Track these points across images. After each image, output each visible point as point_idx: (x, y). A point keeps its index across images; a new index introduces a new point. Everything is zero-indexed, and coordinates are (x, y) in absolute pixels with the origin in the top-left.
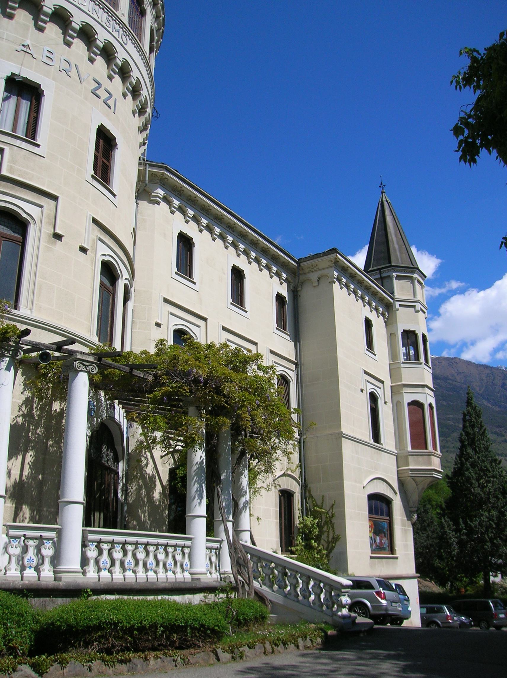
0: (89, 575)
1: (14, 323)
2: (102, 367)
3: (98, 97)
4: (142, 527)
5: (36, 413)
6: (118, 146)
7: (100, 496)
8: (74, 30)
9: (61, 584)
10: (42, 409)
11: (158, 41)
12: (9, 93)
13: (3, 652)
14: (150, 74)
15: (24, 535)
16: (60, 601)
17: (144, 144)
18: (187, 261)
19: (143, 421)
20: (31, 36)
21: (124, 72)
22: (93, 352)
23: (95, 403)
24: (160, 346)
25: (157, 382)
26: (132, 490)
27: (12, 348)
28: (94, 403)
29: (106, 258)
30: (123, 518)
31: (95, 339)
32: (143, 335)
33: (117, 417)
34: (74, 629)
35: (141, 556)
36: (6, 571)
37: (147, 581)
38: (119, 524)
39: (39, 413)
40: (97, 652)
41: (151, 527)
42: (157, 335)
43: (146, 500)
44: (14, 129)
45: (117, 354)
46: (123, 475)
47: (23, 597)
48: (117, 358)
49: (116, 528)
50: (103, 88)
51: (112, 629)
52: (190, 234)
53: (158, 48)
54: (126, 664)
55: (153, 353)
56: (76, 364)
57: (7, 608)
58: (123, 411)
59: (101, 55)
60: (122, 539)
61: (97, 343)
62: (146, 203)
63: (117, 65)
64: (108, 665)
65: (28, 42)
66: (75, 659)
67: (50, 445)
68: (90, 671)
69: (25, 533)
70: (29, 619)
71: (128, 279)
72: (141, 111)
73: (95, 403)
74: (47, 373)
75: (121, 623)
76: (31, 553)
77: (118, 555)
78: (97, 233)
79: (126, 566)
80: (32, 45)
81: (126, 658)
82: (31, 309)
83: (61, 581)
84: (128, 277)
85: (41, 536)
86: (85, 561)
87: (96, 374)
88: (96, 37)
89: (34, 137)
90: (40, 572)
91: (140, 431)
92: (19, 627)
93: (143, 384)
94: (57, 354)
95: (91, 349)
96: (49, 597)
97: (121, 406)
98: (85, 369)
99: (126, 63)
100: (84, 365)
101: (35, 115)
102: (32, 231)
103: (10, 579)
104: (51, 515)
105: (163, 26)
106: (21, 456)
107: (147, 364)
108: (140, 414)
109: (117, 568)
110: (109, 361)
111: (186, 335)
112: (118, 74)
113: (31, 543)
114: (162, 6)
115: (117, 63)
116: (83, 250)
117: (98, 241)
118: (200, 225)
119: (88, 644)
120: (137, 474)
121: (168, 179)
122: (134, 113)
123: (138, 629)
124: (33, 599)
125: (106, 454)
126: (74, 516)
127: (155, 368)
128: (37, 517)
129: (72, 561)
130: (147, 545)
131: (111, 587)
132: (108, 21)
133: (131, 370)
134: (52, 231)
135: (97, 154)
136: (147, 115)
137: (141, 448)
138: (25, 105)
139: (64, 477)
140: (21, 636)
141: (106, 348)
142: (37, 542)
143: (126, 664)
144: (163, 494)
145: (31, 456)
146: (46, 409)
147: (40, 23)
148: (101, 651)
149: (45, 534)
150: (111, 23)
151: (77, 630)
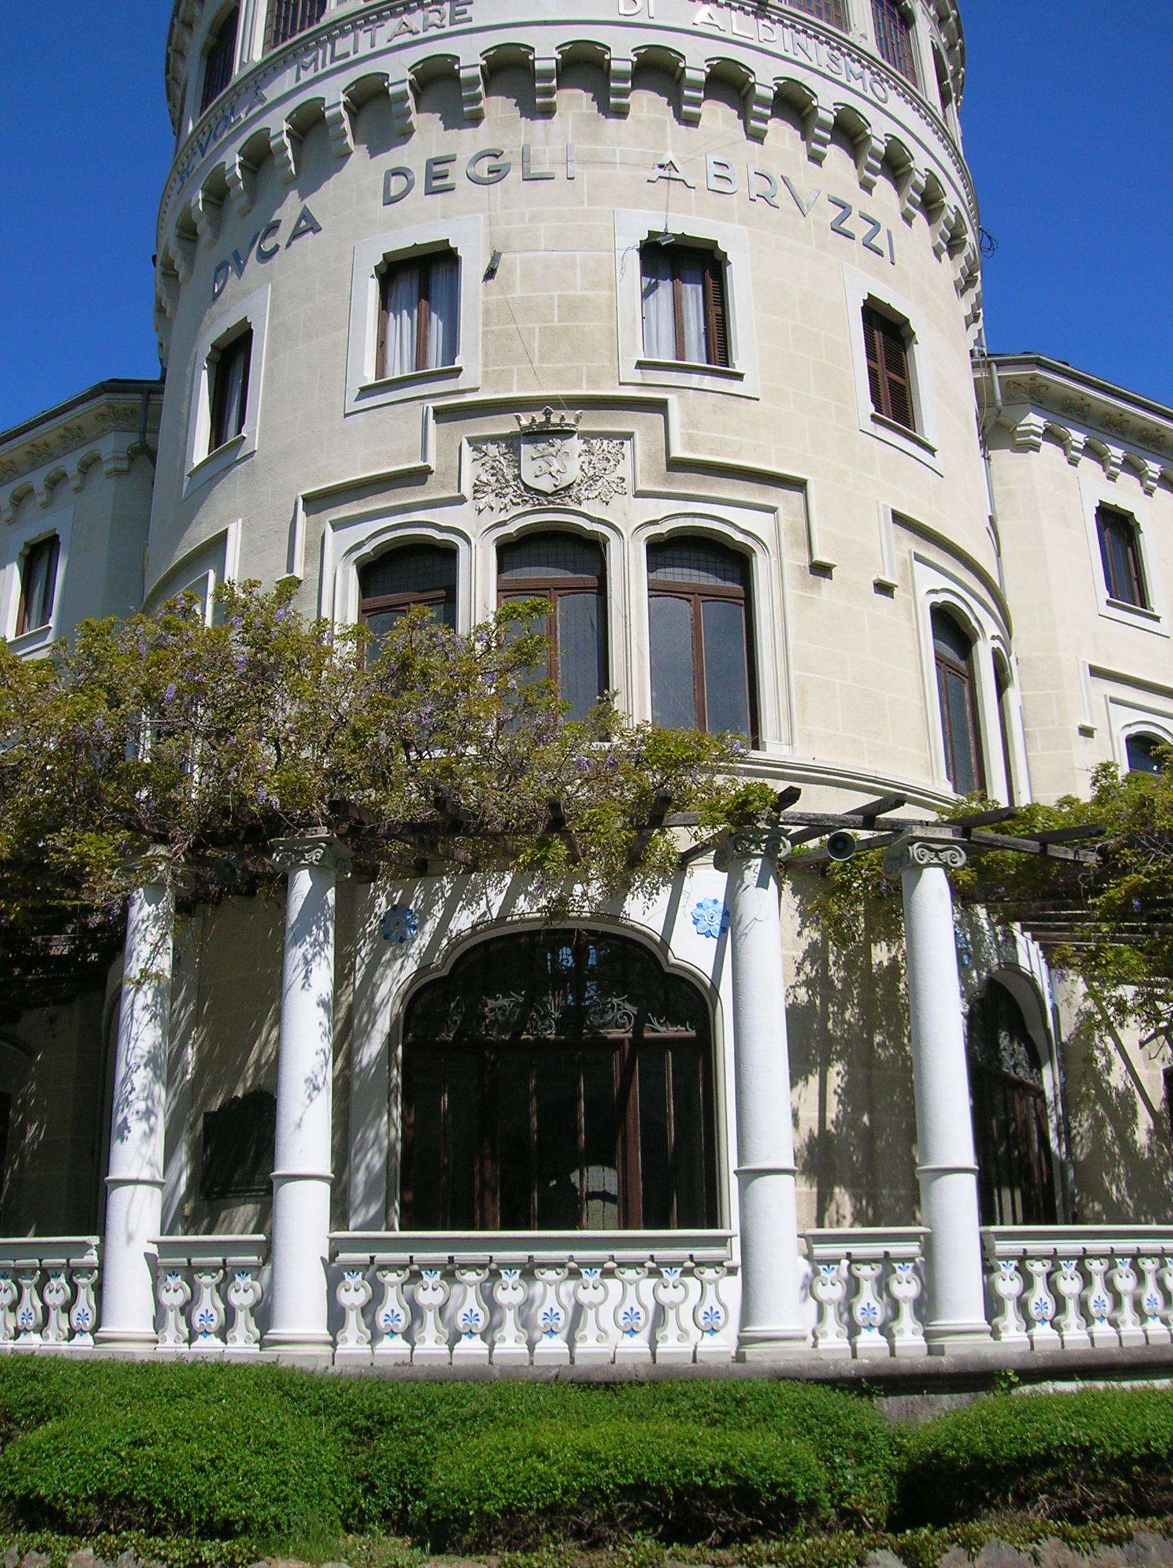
0: (1005, 1337)
1: (760, 780)
2: (974, 849)
3: (849, 236)
4: (1115, 1213)
5: (836, 974)
6: (918, 337)
7: (1009, 1150)
8: (762, 102)
9: (945, 1362)
10: (849, 965)
12: (652, 277)
13: (831, 1523)
15: (849, 1255)
16: (946, 1401)
17: (976, 318)
18: (1130, 573)
19: (1091, 965)
20: (675, 142)
21: (895, 165)
22: (946, 818)
23: (968, 936)
24: (1104, 781)
25: (1111, 866)
26: (1081, 1130)
27: (765, 837)
28: (964, 936)
29: (940, 598)
30: (1068, 1198)
31: (945, 788)
32: (1056, 761)
33: (1023, 961)
34: (988, 1466)
35: (1126, 1283)
36: (816, 1338)
37: (1121, 1344)
38: (1060, 1213)
39: (842, 974)
40: (1049, 1517)
41: (1138, 1212)
42: (1091, 755)
43: (1117, 1151)
44: (680, 351)
45: (1005, 815)
46: (1055, 1096)
47: (860, 1395)
48: (1005, 823)
49: (1055, 1223)
50: (855, 213)
51: (1077, 1463)
52: (1125, 504)
53: (960, 89)
54: (1122, 1546)
55: (1089, 800)
56: (914, 850)
57: (830, 1422)
58: (1035, 947)
60: (1074, 1246)
61: (954, 796)
62: (1006, 453)
64: (1078, 1549)
65: (668, 157)
66: (997, 1534)
67: (878, 1044)
68: (1037, 1562)
69: (652, 1253)
70: (881, 1444)
71: (998, 638)
72: (954, 244)
73: (968, 936)
74: (849, 880)
75: (1098, 1447)
77: (1070, 1285)
78: (910, 543)
79: (1093, 1310)
81: (1120, 1532)
82: (791, 743)
83: (943, 1354)
84: (997, 633)
85: (887, 1254)
86: (993, 1306)
87: (962, 868)
88: (814, 103)
89: (725, 359)
90: (894, 1336)
91: (1081, 988)
92: (860, 1464)
93: (1076, 877)
94: (864, 835)
95: (942, 811)
96: (919, 1392)
97: (1028, 934)
98: (936, 861)
99: (894, 144)
100: (931, 850)
102: (762, 569)
103: (827, 1357)
104: (901, 1205)
106: (817, 1077)
107: (1079, 829)
108: (1079, 948)
109: (1072, 1316)
110: (987, 833)
111: (1157, 744)
112: (882, 172)
113: (865, 1271)
115: (873, 149)
116: (884, 588)
117: (915, 563)
118: (1145, 478)
119: (1024, 1499)
120: (1088, 1090)
121: (1047, 387)
122: (937, 253)
123: (1142, 1461)
124: (884, 1400)
125: (1011, 1052)
126: (956, 1200)
127: (1101, 833)
128: (870, 1212)
129: (963, 1305)
130: (1136, 1256)
131: (1063, 1363)
132: (834, 60)
133: (1044, 846)
134: (807, 559)
135: (873, 365)
136: (967, 250)
137: (1091, 1028)
138: (692, 294)
139: (923, 1114)
140: (868, 1486)
141: (974, 805)
142: (878, 1268)
143: (1122, 1546)
144: (1156, 1132)
145: (838, 1074)
146: (857, 963)
147: (685, 108)
148: (1056, 1515)
149: (896, 1249)
150: (841, 62)
151: (997, 1467)
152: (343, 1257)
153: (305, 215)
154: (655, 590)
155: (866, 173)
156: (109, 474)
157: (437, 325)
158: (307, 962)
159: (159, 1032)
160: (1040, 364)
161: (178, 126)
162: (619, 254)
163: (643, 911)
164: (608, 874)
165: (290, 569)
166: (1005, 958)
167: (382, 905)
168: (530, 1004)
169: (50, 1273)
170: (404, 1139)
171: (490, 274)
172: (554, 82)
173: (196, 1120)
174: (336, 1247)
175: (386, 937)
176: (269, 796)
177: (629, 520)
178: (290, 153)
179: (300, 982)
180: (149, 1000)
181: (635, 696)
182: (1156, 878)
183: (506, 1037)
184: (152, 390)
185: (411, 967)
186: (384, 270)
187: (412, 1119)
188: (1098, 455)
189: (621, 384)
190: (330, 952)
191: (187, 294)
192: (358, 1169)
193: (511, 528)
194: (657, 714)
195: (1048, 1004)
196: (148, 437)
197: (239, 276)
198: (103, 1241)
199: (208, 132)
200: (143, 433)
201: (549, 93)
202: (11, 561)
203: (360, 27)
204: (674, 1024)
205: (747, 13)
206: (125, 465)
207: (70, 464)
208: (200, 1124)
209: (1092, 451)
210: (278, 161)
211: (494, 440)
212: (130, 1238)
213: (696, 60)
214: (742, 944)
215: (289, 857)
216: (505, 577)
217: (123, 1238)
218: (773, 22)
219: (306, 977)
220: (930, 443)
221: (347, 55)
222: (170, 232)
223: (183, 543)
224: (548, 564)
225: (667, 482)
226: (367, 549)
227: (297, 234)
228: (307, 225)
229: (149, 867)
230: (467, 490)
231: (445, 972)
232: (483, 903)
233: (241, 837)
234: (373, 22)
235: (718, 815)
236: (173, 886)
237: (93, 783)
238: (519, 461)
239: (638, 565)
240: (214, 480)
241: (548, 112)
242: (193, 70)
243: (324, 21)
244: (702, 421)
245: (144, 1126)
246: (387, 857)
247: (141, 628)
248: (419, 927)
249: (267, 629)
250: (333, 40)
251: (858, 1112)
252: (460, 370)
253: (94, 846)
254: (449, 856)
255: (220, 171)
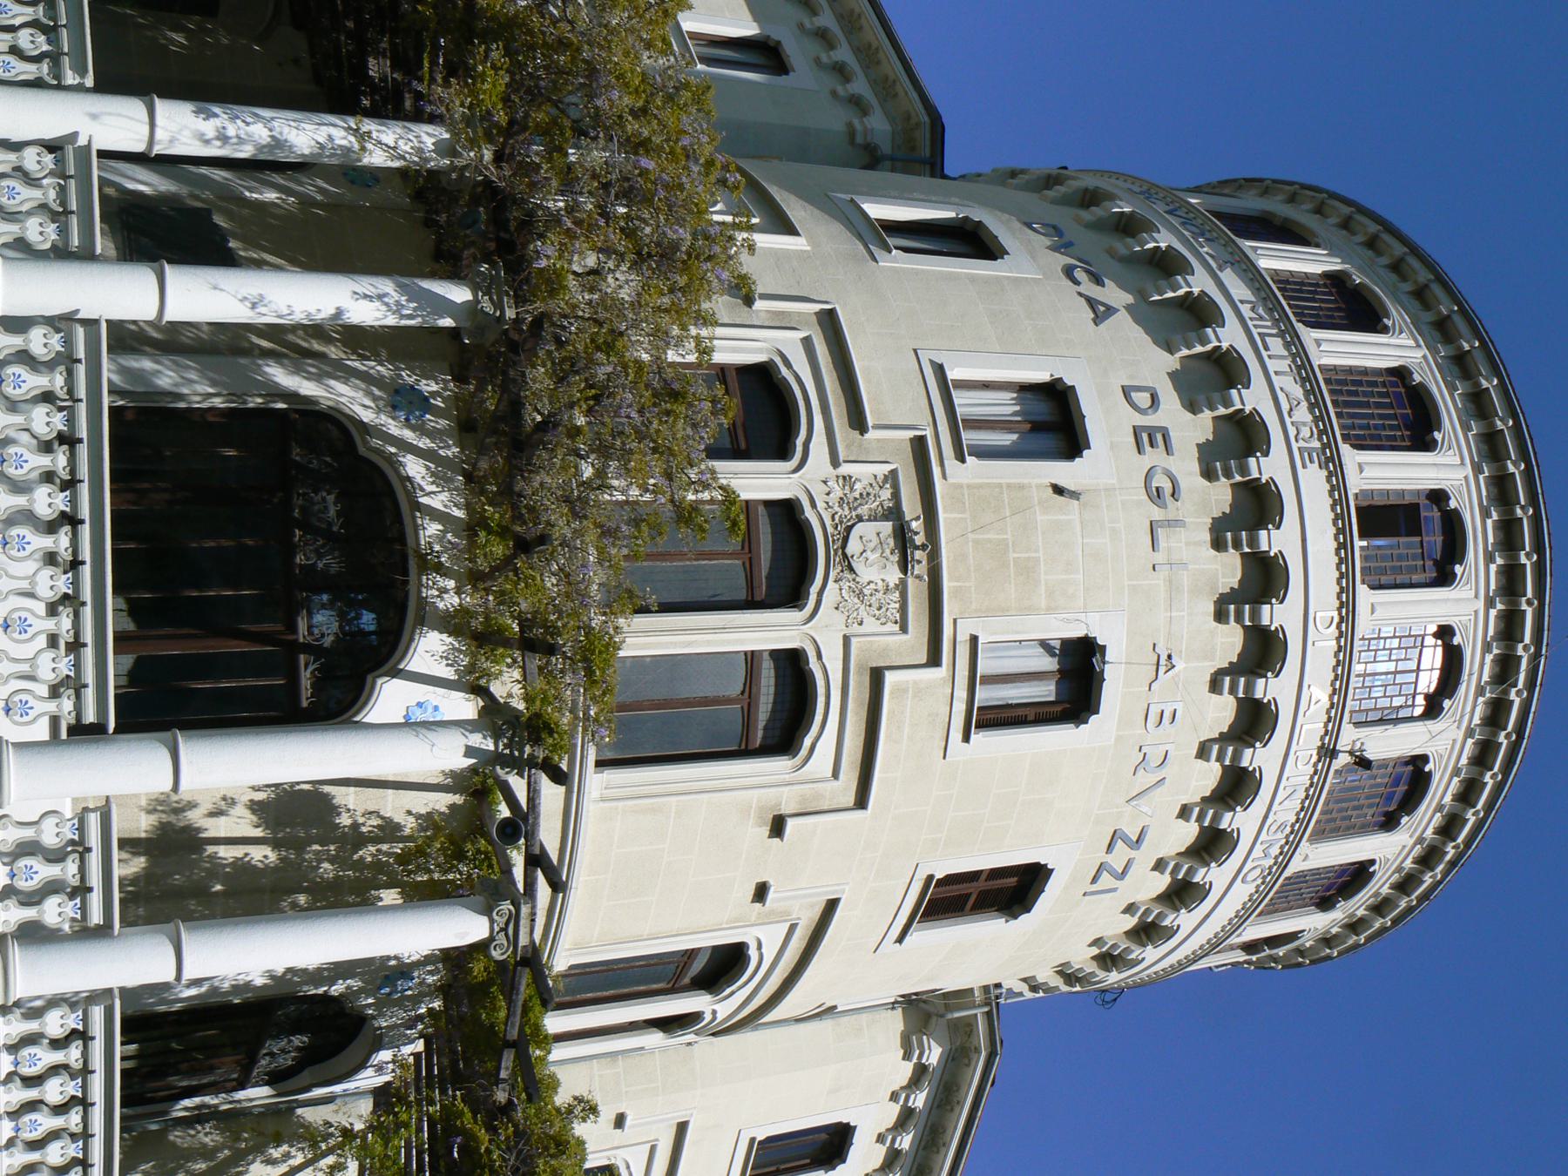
2: (504, 974)
5: (367, 853)
8: (1237, 756)
10: (378, 866)
11: (1275, 959)
14: (1196, 958)
17: (1034, 989)
20: (1195, 669)
21: (1182, 893)
25: (496, 1115)
29: (753, 953)
44: (990, 680)
46: (239, 1101)
50: (1133, 854)
56: (506, 906)
59: (1202, 829)
62: (900, 1026)
63: (1191, 871)
65: (1180, 665)
72: (1108, 960)
76: (45, 871)
78: (807, 918)
79: (26, 1118)
80: (1177, 675)
82: (603, 800)
84: (720, 1017)
88: (1238, 809)
89: (982, 725)
99: (1201, 892)
101: (1031, 718)
105: (1313, 962)
112: (1174, 881)
114: (1356, 946)
116: (761, 892)
120: (246, 1140)
121: (968, 1065)
122: (1097, 942)
125: (283, 1049)
126: (141, 963)
127: (530, 1099)
132: (1281, 827)
135: (983, 877)
136: (1101, 974)
138: (1045, 691)
147: (1227, 679)
152: (80, 332)
153: (1110, 311)
154: (752, 658)
155: (1172, 864)
156: (850, 125)
157: (1006, 439)
158: (380, 297)
159: (307, 152)
160: (992, 1055)
161: (1197, 190)
162: (1082, 616)
163: (430, 650)
164: (462, 611)
165: (764, 297)
166: (386, 1035)
167: (429, 386)
168: (330, 537)
169: (52, 35)
170: (190, 410)
171: (1058, 490)
172: (1247, 550)
173: (203, 201)
174: (91, 324)
175: (397, 392)
176: (545, 254)
177: (822, 629)
178: (1170, 295)
179: (360, 290)
180: (339, 142)
181: (647, 638)
182: (485, 1159)
183: (296, 513)
184: (934, 166)
185: (367, 416)
186: (1059, 387)
187: (211, 419)
188: (902, 1123)
189: (955, 621)
190: (391, 320)
191: (1031, 200)
192: (157, 362)
193: (809, 513)
194: (628, 663)
195: (337, 1089)
196: (888, 164)
197: (1049, 248)
198: (88, 90)
199: (1189, 218)
200: (892, 159)
201: (1237, 545)
202: (761, 27)
203: (1294, 361)
204: (313, 686)
205: (1322, 739)
206: (859, 140)
207: (860, 86)
208: (198, 204)
209: (906, 1115)
210: (1162, 283)
211: (896, 495)
212: (94, 117)
213: (1274, 688)
214: (406, 741)
215: (484, 280)
216: (761, 509)
217: (94, 110)
218: (1315, 765)
219: (366, 296)
220: (908, 938)
221: (1267, 349)
222: (1090, 182)
223: (786, 194)
224: (774, 551)
225: (860, 667)
226: (784, 371)
227: (1092, 303)
228: (1101, 312)
229: (473, 143)
230: (845, 469)
231: (362, 450)
232: (433, 488)
233: (502, 234)
234: (1299, 374)
235: (538, 703)
236: (453, 168)
237: (551, 90)
238: (875, 520)
239: (777, 640)
240: (849, 224)
241: (1218, 544)
242: (1250, 203)
243: (1299, 327)
244: (922, 701)
245: (211, 134)
246: (481, 388)
247: (705, 139)
248: (407, 423)
249: (709, 258)
250: (1281, 334)
251: (225, 879)
252: (963, 461)
253: (493, 85)
254: (482, 450)
255: (1150, 227)
